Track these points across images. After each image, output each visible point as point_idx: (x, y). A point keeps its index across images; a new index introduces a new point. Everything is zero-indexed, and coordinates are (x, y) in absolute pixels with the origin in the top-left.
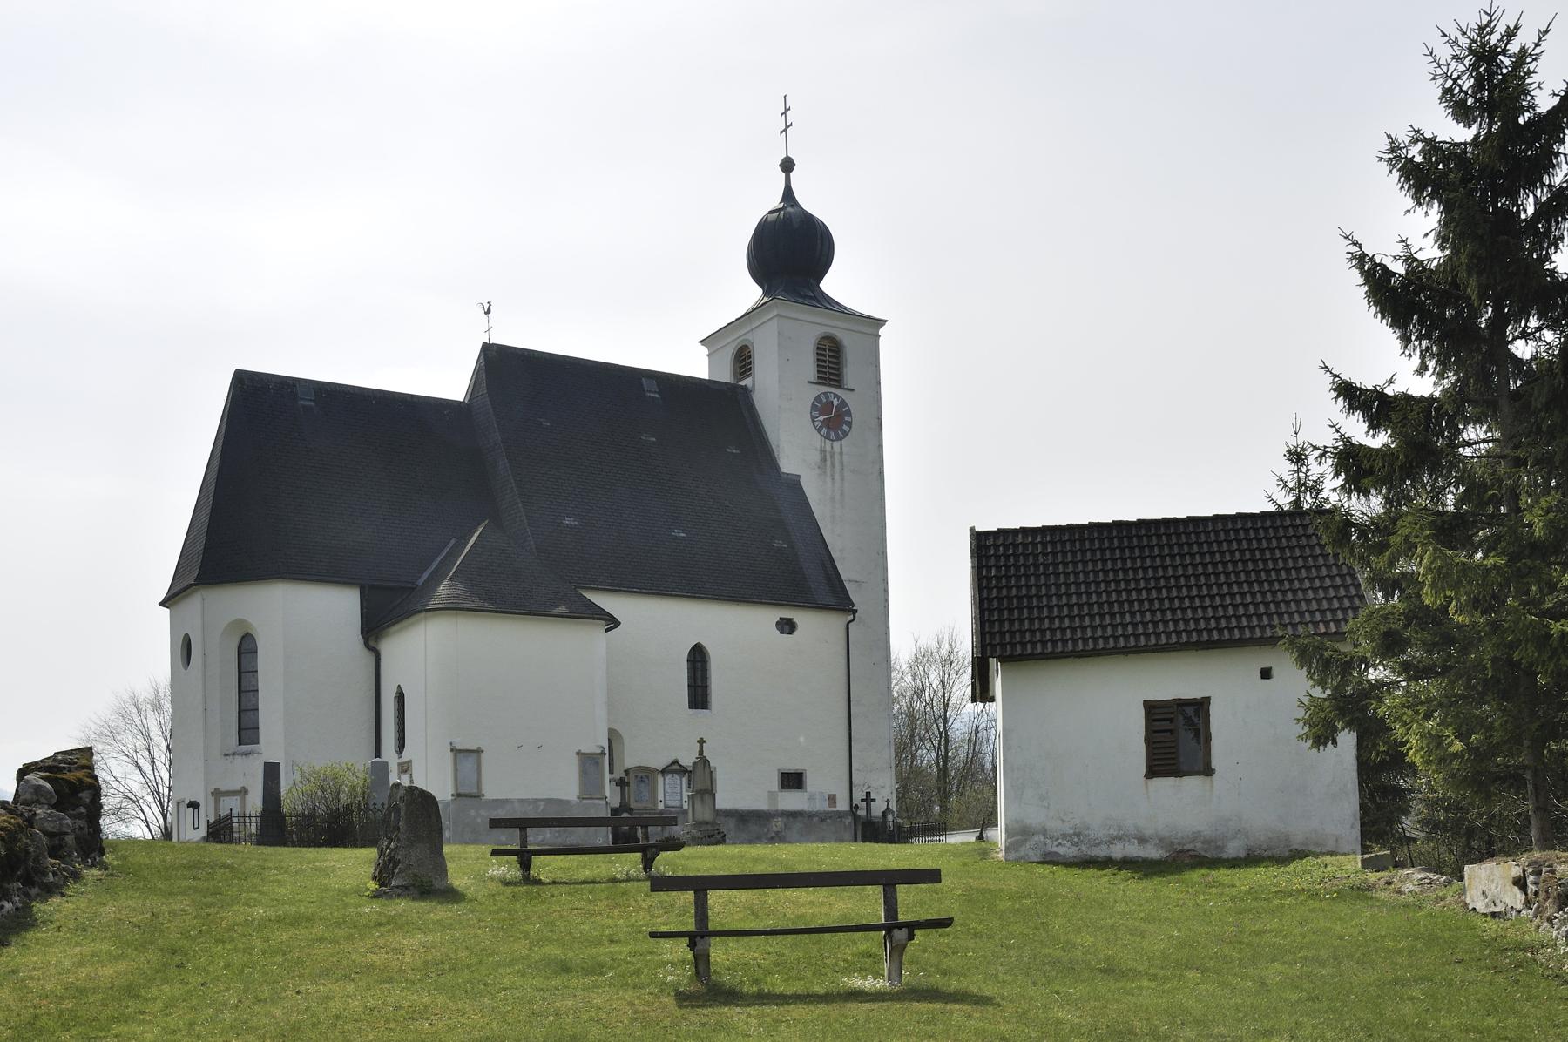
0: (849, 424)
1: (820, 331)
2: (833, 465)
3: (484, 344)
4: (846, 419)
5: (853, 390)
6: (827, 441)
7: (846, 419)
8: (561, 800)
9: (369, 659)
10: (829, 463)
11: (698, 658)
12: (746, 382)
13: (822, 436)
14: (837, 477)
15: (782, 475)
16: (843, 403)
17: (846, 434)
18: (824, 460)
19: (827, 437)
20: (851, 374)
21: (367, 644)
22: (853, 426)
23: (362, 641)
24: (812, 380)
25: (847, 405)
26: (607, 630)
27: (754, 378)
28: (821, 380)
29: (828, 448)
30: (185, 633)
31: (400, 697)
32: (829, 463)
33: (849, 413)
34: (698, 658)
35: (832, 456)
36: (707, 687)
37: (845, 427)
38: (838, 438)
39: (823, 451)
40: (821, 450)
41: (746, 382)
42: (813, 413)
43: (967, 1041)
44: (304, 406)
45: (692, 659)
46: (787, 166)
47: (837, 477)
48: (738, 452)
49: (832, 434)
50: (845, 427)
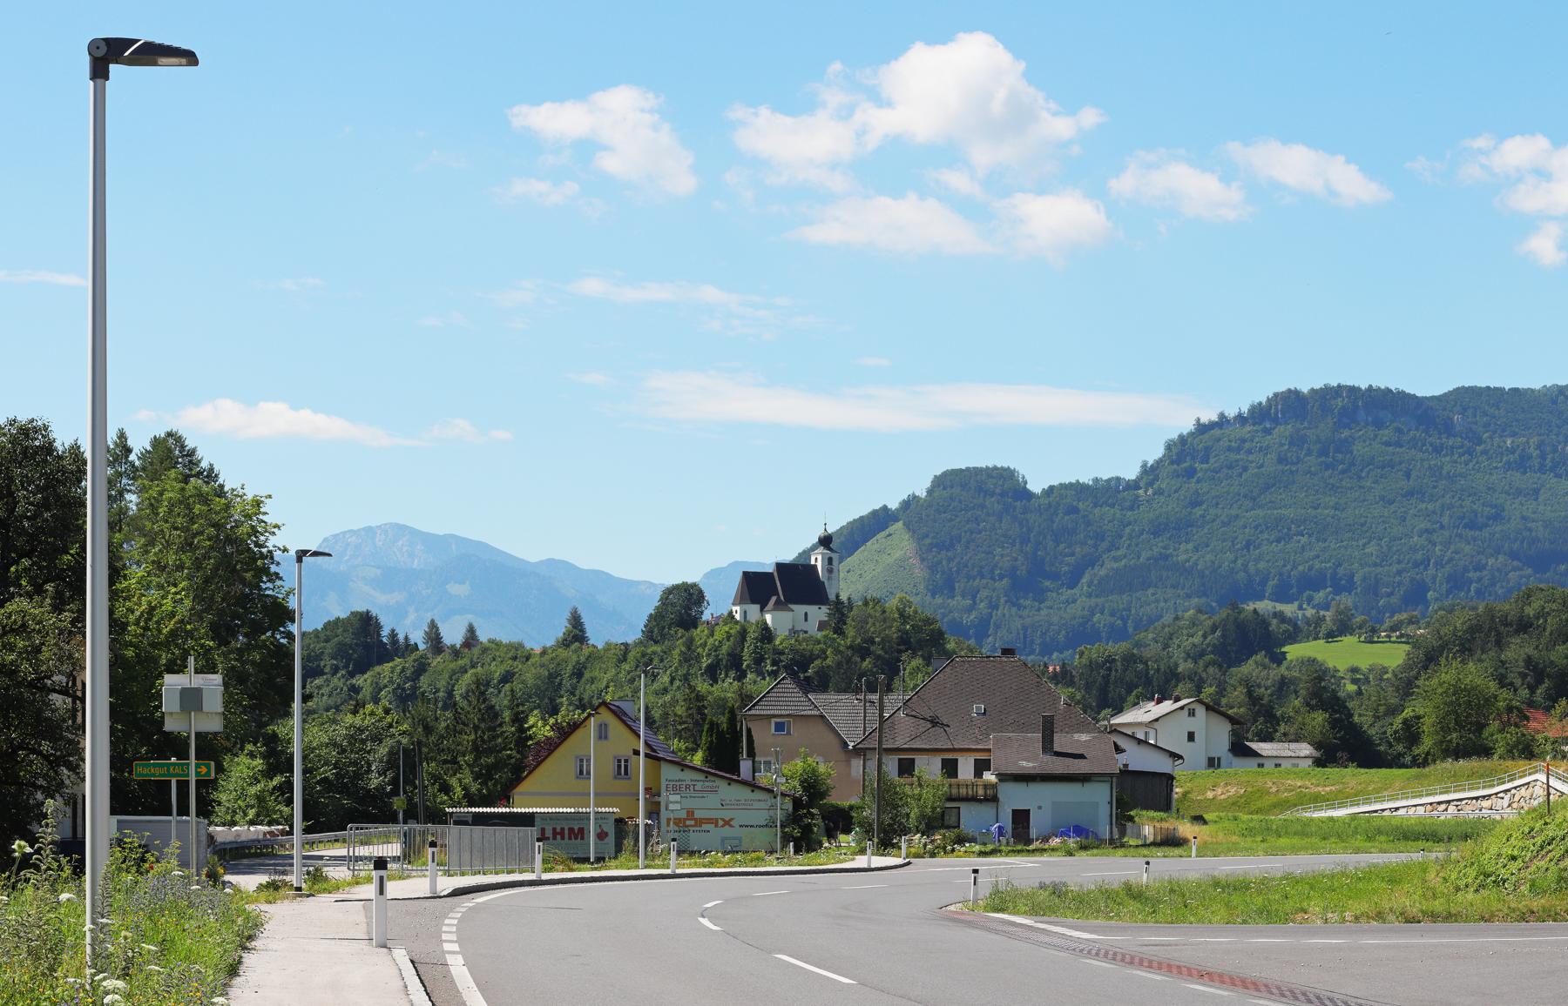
11: (806, 614)
34: (806, 614)
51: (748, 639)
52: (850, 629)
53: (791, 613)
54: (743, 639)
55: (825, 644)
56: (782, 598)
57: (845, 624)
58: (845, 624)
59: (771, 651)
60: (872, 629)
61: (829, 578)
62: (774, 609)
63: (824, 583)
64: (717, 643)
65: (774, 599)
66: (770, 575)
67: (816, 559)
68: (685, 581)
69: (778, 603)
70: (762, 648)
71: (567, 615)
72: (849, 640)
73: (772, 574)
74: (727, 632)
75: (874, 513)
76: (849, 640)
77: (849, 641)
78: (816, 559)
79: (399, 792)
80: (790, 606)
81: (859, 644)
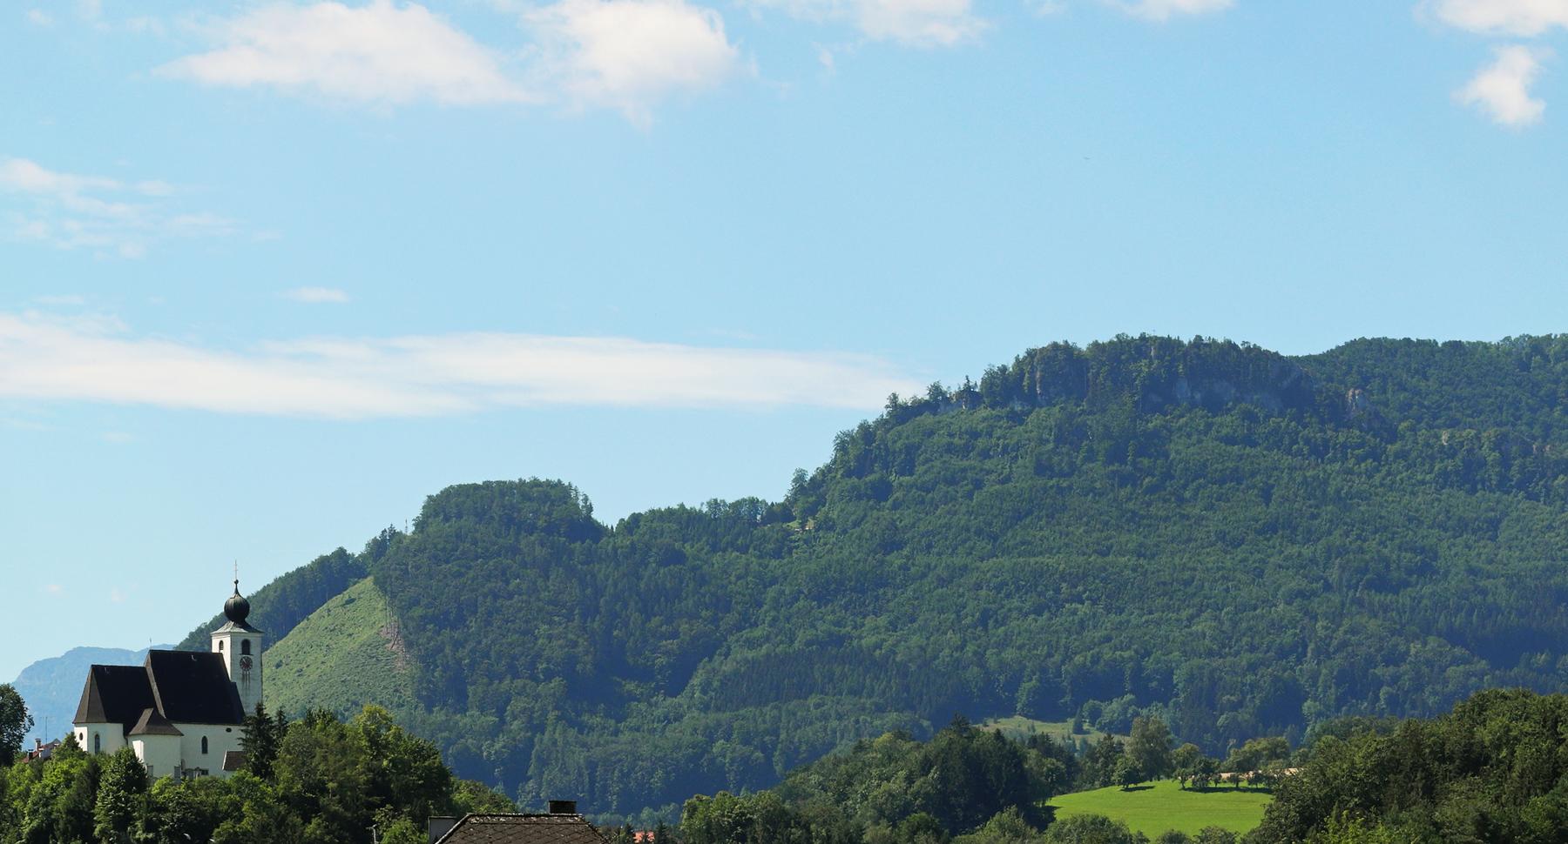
11: (205, 740)
34: (205, 740)
39: (243, 675)
46: (237, 582)
51: (103, 784)
53: (179, 739)
56: (162, 712)
58: (274, 757)
59: (144, 805)
60: (321, 767)
61: (244, 678)
65: (147, 714)
67: (221, 643)
72: (281, 786)
73: (143, 669)
78: (221, 643)
80: (174, 725)
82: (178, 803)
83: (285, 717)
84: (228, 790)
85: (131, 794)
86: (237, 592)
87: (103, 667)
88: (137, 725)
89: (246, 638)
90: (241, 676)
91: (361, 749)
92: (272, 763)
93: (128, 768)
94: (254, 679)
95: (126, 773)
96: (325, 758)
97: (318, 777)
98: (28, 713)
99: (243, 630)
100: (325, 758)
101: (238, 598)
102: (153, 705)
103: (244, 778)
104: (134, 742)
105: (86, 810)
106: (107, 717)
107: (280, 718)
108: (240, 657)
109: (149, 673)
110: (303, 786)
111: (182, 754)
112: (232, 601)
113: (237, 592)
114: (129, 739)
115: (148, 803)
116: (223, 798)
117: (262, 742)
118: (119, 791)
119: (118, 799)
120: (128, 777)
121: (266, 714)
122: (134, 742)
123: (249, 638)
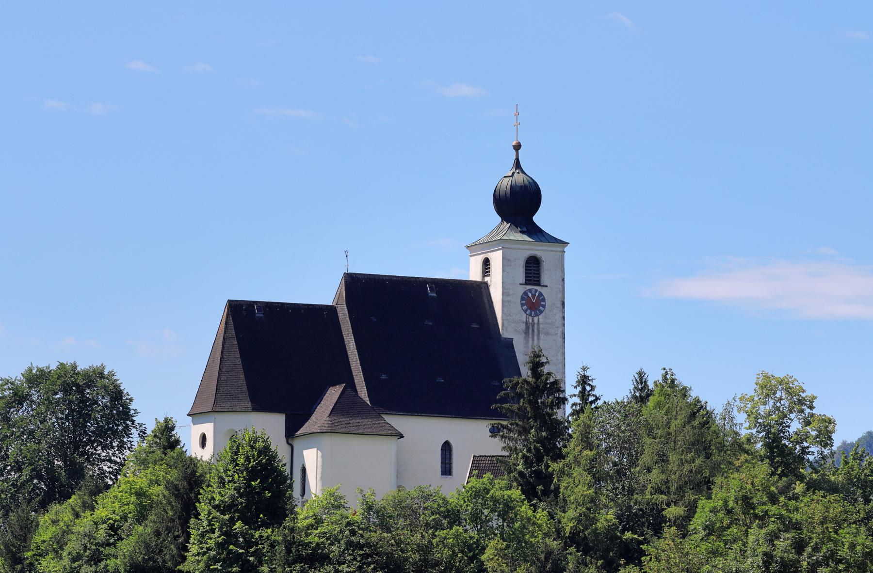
0: (544, 306)
1: (527, 254)
2: (533, 331)
3: (345, 274)
4: (542, 303)
5: (547, 286)
6: (530, 317)
7: (542, 303)
8: (502, 282)
9: (288, 448)
10: (530, 330)
11: (447, 448)
12: (487, 279)
13: (527, 314)
14: (536, 338)
15: (502, 339)
16: (541, 294)
17: (541, 312)
18: (527, 328)
19: (530, 315)
20: (545, 278)
21: (288, 442)
22: (546, 306)
23: (285, 440)
24: (521, 282)
25: (543, 295)
26: (398, 438)
27: (491, 278)
28: (528, 282)
29: (531, 321)
30: (204, 450)
31: (304, 470)
32: (530, 330)
33: (544, 300)
34: (447, 448)
35: (533, 326)
36: (451, 464)
37: (541, 308)
38: (536, 315)
39: (527, 323)
40: (526, 323)
41: (487, 279)
42: (522, 302)
43: (629, 572)
44: (258, 317)
45: (444, 448)
46: (517, 147)
47: (536, 338)
48: (478, 326)
49: (533, 313)
50: (541, 308)
51: (203, 508)
52: (577, 472)
53: (393, 442)
54: (188, 510)
55: (476, 518)
56: (363, 392)
57: (559, 456)
58: (559, 456)
59: (281, 549)
60: (656, 476)
61: (529, 329)
62: (332, 431)
63: (509, 344)
64: (101, 534)
65: (333, 394)
66: (325, 313)
67: (486, 263)
68: (68, 360)
69: (343, 408)
70: (248, 544)
71: (633, 373)
72: (571, 513)
73: (331, 311)
74: (140, 494)
75: (205, 444)
76: (571, 513)
77: (568, 520)
78: (486, 263)
79: (530, 284)
80: (384, 416)
81: (610, 531)
82: (350, 544)
83: (593, 388)
84: (453, 517)
85: (257, 529)
86: (518, 165)
87: (250, 305)
88: (313, 417)
89: (533, 253)
90: (523, 327)
91: (740, 446)
92: (555, 467)
93: (253, 474)
94: (547, 334)
95: (248, 485)
96: (663, 459)
97: (648, 497)
98: (138, 419)
99: (526, 238)
100: (663, 459)
101: (519, 178)
102: (346, 378)
103: (488, 491)
104: (305, 452)
105: (169, 564)
106: (252, 400)
107: (584, 389)
108: (522, 290)
109: (341, 317)
110: (619, 517)
111: (398, 477)
112: (506, 183)
113: (518, 165)
114: (297, 443)
115: (289, 545)
116: (441, 533)
117: (539, 429)
118: (232, 521)
119: (230, 536)
120: (248, 492)
121: (549, 374)
122: (305, 452)
123: (538, 254)
